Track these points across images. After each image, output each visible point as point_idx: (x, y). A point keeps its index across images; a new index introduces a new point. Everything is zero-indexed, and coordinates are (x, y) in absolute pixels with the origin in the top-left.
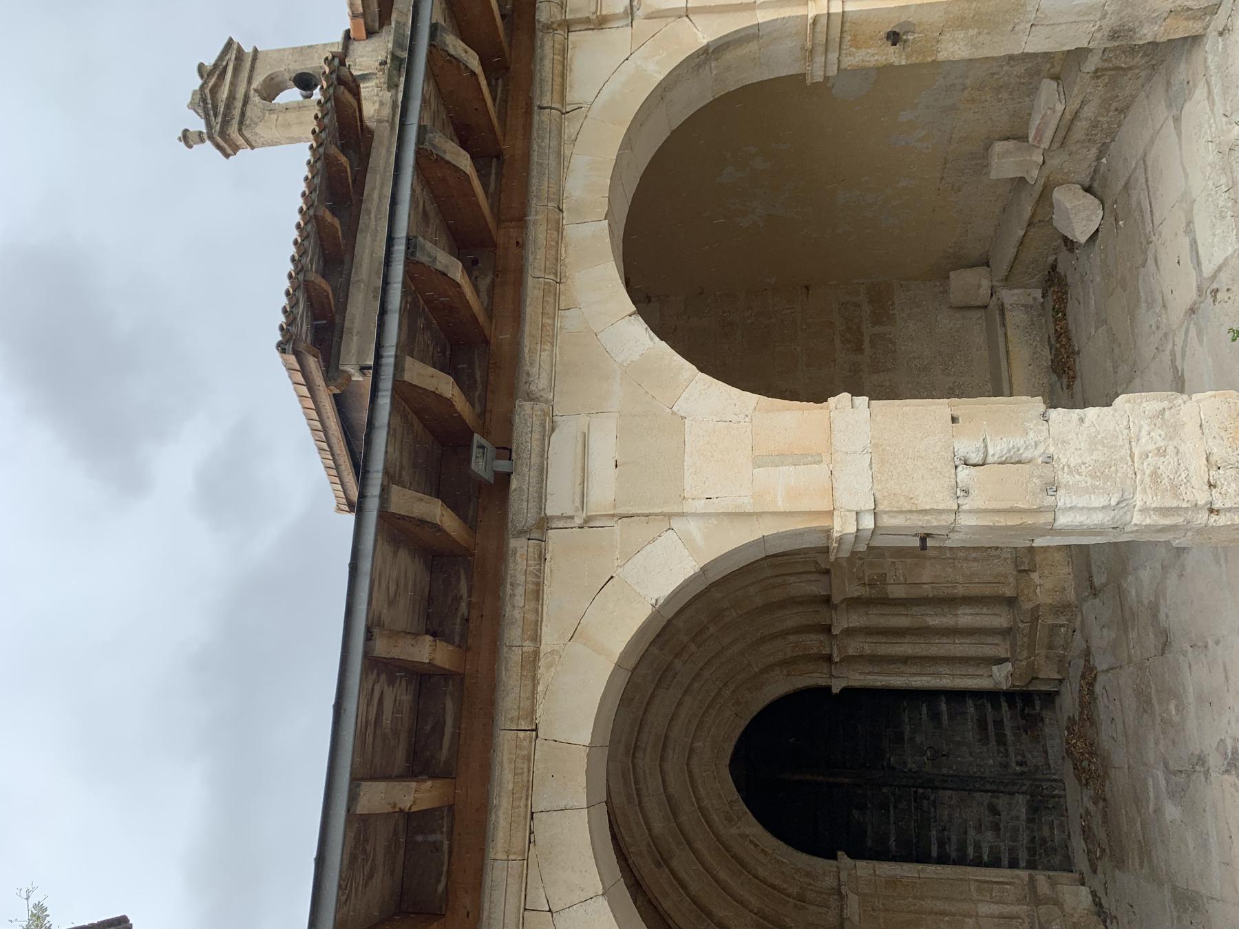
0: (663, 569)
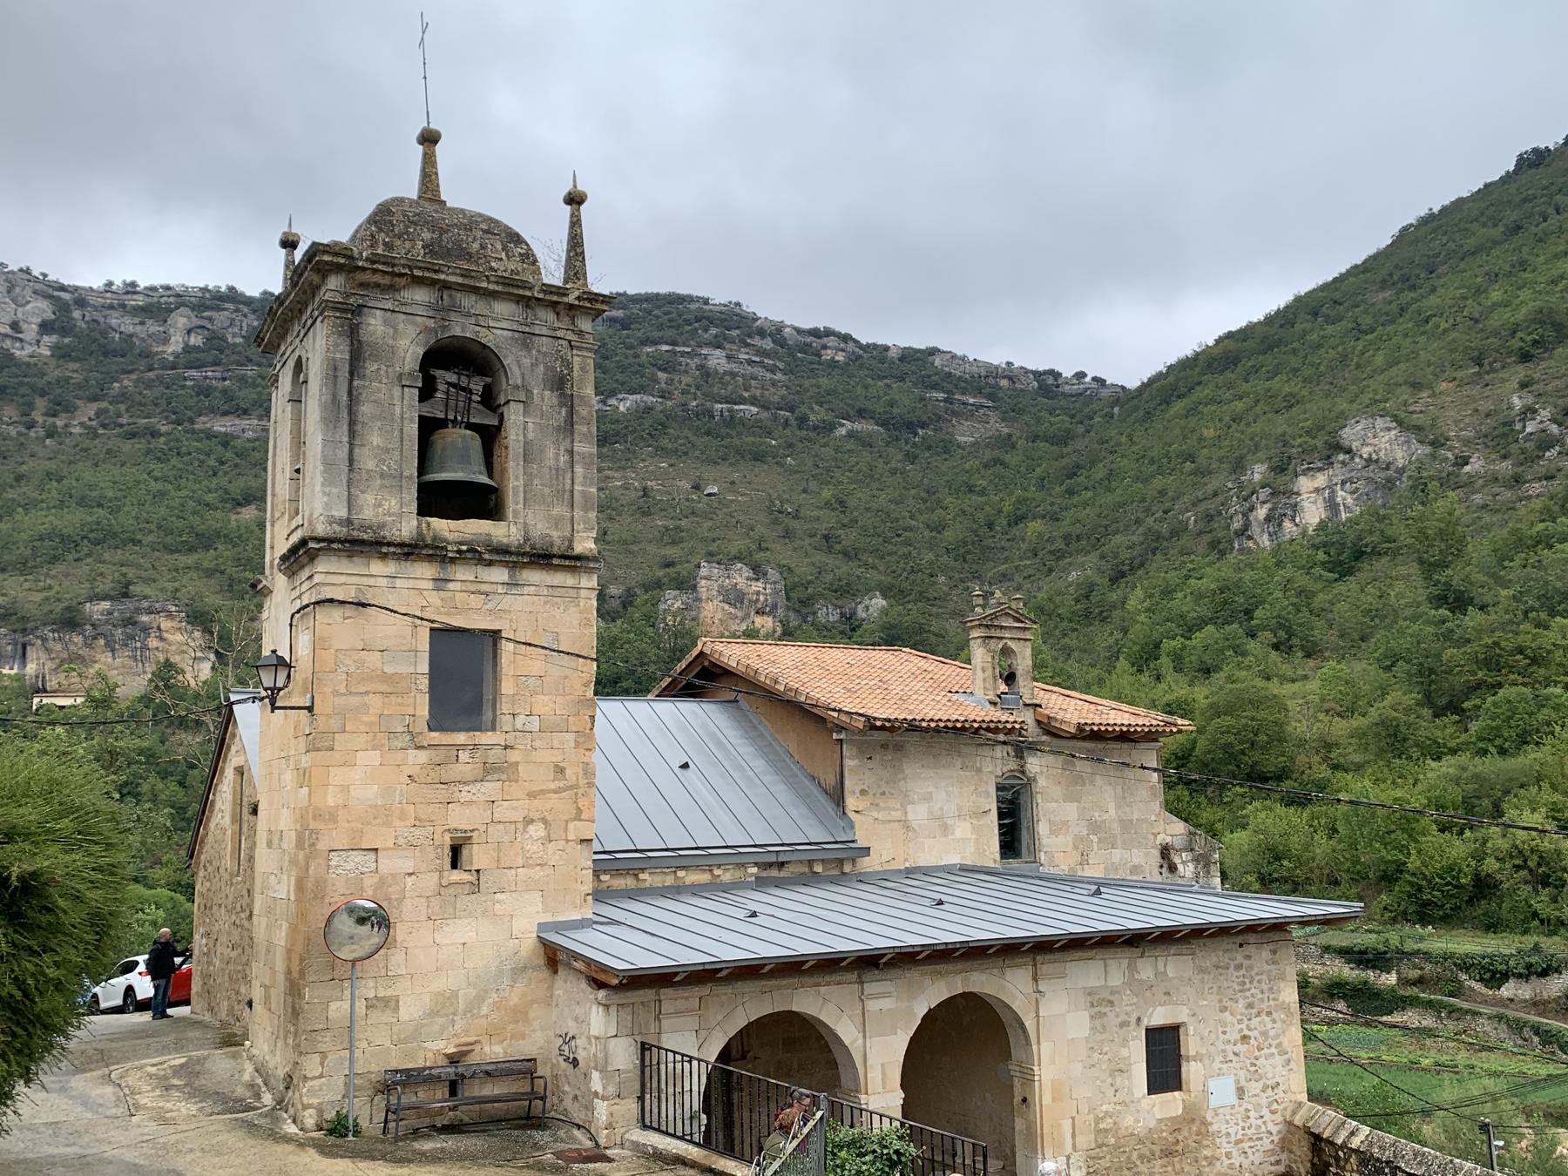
0: (846, 1031)
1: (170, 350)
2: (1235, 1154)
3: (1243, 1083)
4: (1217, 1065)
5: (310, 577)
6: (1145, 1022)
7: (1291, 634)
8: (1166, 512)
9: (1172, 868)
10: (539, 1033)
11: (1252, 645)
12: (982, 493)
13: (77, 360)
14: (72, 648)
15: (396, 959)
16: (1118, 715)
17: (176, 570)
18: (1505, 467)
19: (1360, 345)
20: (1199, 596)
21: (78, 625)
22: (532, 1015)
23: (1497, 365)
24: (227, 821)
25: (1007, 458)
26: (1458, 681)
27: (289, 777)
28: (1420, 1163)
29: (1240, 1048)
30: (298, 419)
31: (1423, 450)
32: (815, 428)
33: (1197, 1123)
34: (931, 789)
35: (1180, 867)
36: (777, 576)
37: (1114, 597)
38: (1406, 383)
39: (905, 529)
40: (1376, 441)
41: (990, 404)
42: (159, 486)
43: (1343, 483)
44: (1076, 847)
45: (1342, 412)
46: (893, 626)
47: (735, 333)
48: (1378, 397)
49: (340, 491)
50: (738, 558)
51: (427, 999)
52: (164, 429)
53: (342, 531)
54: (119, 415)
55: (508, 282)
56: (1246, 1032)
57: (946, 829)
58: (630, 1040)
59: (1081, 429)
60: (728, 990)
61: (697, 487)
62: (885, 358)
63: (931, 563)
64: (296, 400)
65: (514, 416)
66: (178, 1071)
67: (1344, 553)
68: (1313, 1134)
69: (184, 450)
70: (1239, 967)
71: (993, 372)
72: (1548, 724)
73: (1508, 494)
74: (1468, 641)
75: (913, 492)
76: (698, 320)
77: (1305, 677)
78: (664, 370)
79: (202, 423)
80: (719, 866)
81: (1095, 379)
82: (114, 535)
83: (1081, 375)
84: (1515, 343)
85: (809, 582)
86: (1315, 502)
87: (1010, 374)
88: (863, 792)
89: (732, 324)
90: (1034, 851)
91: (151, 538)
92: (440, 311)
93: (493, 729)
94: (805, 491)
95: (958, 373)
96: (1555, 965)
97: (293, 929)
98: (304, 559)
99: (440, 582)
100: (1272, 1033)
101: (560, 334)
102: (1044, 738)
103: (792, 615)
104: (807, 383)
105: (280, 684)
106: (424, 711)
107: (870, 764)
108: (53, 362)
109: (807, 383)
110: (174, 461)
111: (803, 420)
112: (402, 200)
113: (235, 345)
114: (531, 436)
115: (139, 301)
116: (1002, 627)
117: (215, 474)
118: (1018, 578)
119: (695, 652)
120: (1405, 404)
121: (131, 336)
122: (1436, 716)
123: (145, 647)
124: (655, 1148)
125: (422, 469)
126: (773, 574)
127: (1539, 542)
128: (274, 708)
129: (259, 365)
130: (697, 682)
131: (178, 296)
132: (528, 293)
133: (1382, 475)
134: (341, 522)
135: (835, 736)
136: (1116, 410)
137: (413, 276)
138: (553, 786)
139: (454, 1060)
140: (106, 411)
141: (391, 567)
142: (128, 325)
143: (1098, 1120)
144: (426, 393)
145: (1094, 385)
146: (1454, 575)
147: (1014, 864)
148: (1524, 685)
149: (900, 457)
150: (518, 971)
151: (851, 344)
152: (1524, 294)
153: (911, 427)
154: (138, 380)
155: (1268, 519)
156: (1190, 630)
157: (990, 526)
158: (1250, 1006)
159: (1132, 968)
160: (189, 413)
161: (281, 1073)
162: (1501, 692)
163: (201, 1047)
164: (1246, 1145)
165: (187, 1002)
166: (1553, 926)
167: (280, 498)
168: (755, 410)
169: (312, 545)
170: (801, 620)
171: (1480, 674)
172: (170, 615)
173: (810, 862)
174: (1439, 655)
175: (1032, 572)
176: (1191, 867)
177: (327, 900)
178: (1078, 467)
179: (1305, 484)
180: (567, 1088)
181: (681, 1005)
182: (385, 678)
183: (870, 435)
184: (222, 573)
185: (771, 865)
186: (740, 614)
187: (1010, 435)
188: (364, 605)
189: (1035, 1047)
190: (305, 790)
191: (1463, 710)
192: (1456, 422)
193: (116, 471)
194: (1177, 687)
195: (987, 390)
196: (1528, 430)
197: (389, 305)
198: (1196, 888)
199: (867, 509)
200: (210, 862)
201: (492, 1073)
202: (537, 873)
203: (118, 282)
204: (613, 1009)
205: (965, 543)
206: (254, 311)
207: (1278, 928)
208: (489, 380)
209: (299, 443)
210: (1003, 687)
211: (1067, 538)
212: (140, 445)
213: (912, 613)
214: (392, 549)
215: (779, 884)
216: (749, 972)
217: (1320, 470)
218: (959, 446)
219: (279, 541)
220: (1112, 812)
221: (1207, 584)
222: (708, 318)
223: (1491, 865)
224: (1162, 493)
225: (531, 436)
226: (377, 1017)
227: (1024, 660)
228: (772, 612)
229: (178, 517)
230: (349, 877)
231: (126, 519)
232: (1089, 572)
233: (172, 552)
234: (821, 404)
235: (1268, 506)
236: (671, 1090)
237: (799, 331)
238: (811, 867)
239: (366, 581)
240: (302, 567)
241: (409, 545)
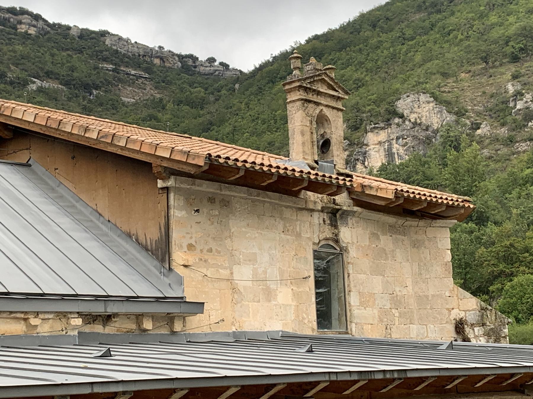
18: (503, 132)
19: (405, 48)
23: (497, 63)
25: (160, 115)
26: (486, 271)
31: (450, 118)
32: (11, 83)
34: (256, 250)
38: (438, 72)
40: (419, 110)
41: (147, 76)
43: (398, 138)
44: (381, 321)
45: (397, 90)
48: (421, 80)
57: (270, 295)
59: (212, 98)
62: (69, 34)
73: (504, 151)
80: (37, 314)
81: (221, 64)
83: (212, 60)
84: (508, 50)
86: (378, 151)
87: (161, 55)
95: (123, 51)
102: (356, 208)
107: (198, 217)
116: (319, 93)
120: (439, 86)
127: (527, 182)
133: (423, 134)
135: (160, 184)
136: (237, 86)
145: (221, 68)
147: (329, 334)
151: (41, 22)
152: (511, 19)
153: (87, 87)
162: (516, 279)
174: (472, 254)
178: (211, 124)
179: (372, 138)
183: (56, 91)
187: (161, 100)
192: (472, 100)
195: (145, 65)
196: (518, 107)
217: (382, 129)
218: (123, 104)
220: (410, 288)
234: (17, 65)
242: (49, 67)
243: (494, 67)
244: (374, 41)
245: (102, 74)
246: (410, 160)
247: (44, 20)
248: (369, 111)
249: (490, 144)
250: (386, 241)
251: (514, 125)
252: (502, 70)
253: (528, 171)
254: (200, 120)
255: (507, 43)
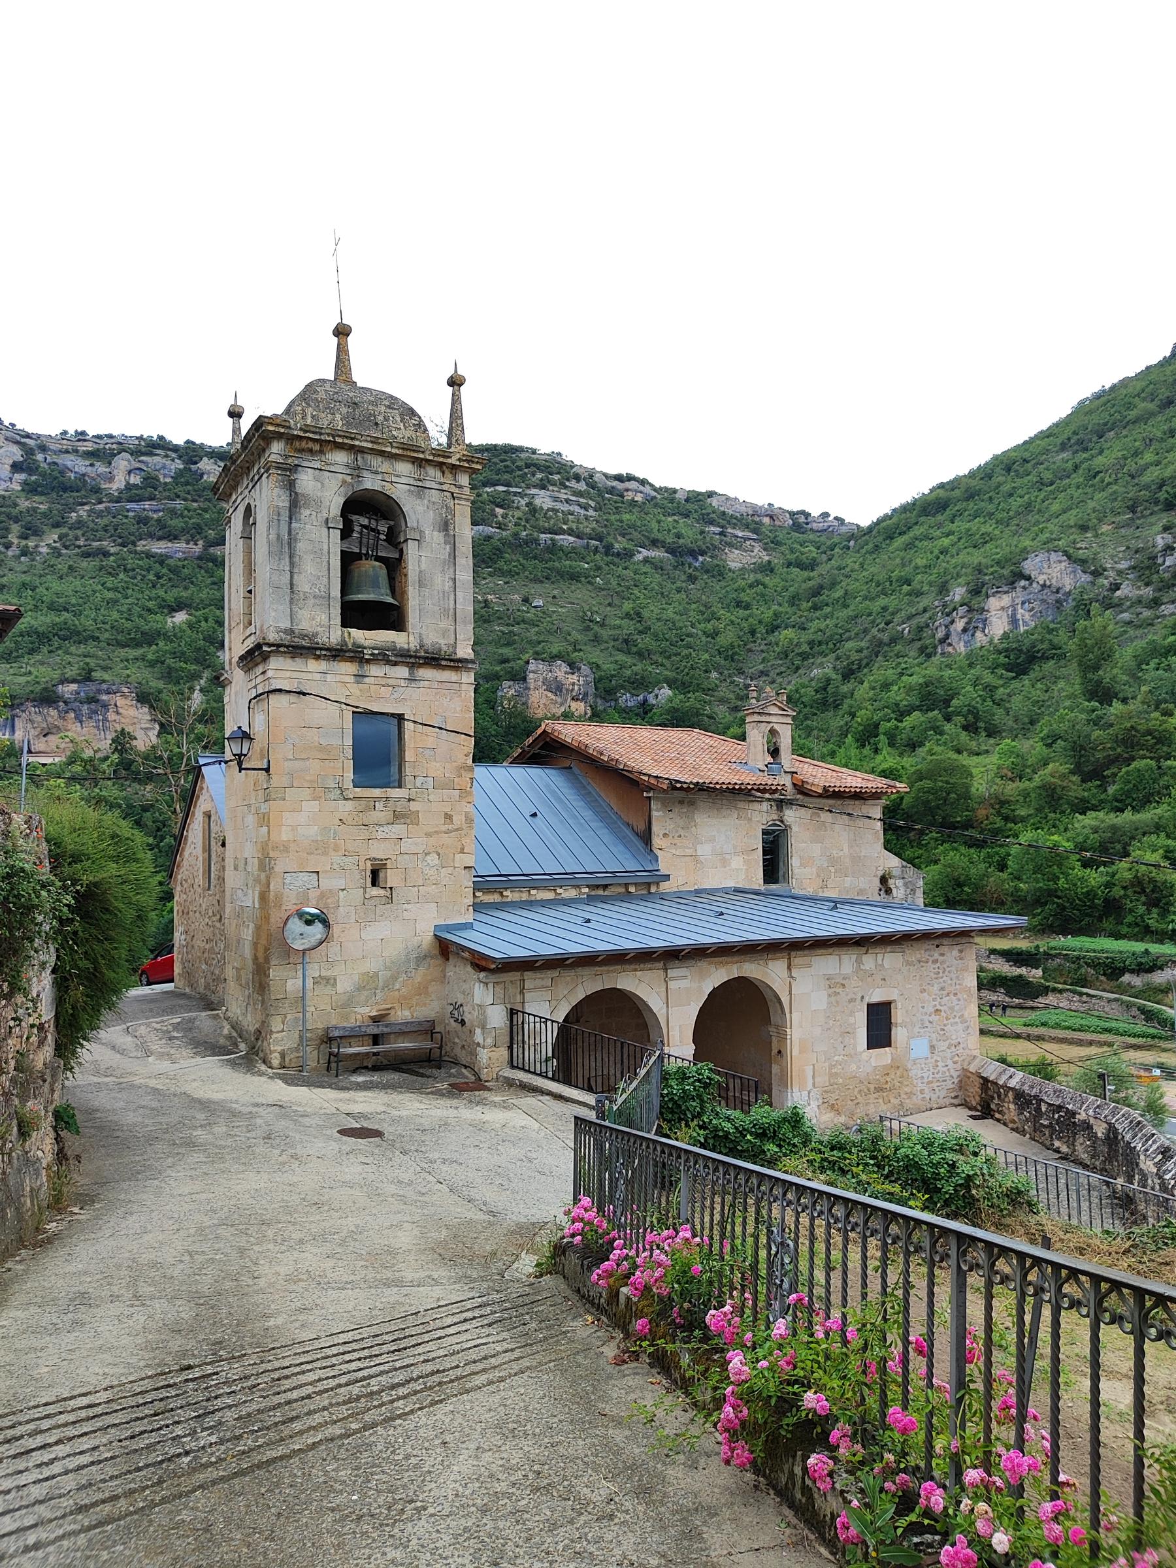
0: (655, 1003)
1: (115, 488)
2: (927, 1091)
3: (935, 1042)
4: (916, 1029)
5: (264, 673)
6: (867, 1000)
7: (977, 717)
8: (887, 624)
9: (888, 891)
10: (436, 1003)
11: (948, 727)
12: (747, 607)
13: (42, 494)
14: (49, 719)
15: (333, 949)
16: (854, 780)
17: (127, 660)
18: (1148, 592)
19: (1042, 495)
20: (910, 689)
21: (55, 702)
22: (430, 989)
24: (199, 851)
25: (767, 580)
27: (251, 820)
28: (1058, 1097)
29: (934, 1018)
30: (249, 553)
32: (618, 554)
33: (901, 1069)
35: (894, 891)
36: (589, 671)
37: (845, 689)
39: (688, 636)
40: (1049, 571)
41: (755, 537)
42: (110, 595)
43: (1023, 603)
44: (818, 876)
45: (1025, 548)
46: (676, 710)
47: (557, 477)
49: (285, 607)
50: (558, 657)
51: (356, 978)
52: (112, 550)
53: (286, 639)
54: (77, 539)
55: (405, 447)
56: (938, 1007)
57: (725, 863)
58: (503, 1007)
60: (572, 973)
61: (526, 600)
63: (706, 661)
64: (247, 537)
65: (411, 549)
66: (176, 1027)
67: (1020, 659)
68: (982, 1078)
69: (129, 566)
70: (936, 961)
71: (756, 511)
72: (1167, 787)
73: (1147, 613)
74: (1112, 725)
75: (694, 606)
76: (528, 466)
77: (987, 752)
78: (501, 507)
79: (142, 546)
80: (561, 887)
81: (836, 518)
82: (78, 633)
83: (825, 515)
85: (613, 676)
87: (772, 513)
88: (665, 835)
89: (553, 470)
90: (787, 880)
91: (107, 635)
92: (356, 471)
93: (400, 787)
94: (610, 605)
95: (731, 512)
96: (1159, 963)
97: (258, 928)
98: (259, 659)
99: (359, 677)
100: (957, 1008)
101: (445, 487)
103: (599, 701)
104: (613, 518)
105: (244, 752)
106: (349, 775)
107: (671, 815)
108: (23, 494)
109: (613, 518)
110: (121, 576)
111: (608, 549)
112: (324, 381)
113: (166, 483)
114: (423, 566)
115: (89, 446)
116: (770, 714)
117: (154, 586)
118: (773, 674)
119: (539, 731)
121: (84, 475)
122: (1083, 781)
123: (105, 720)
124: (521, 1081)
125: (344, 591)
126: (585, 669)
128: (241, 770)
129: (185, 500)
130: (542, 752)
131: (120, 443)
132: (421, 456)
134: (285, 632)
136: (852, 543)
137: (335, 442)
138: (444, 828)
139: (376, 1020)
140: (67, 535)
141: (323, 665)
142: (79, 466)
143: (831, 1067)
144: (346, 534)
145: (836, 523)
146: (1106, 674)
148: (1151, 758)
149: (683, 577)
150: (421, 958)
153: (694, 554)
154: (91, 511)
155: (965, 630)
156: (902, 714)
157: (753, 633)
158: (942, 989)
159: (859, 962)
160: (133, 538)
161: (252, 1029)
163: (190, 1011)
164: (935, 1085)
165: (172, 981)
166: (1162, 937)
167: (234, 612)
168: (572, 539)
169: (265, 648)
170: (609, 700)
171: (1119, 750)
172: (123, 695)
173: (626, 885)
175: (783, 669)
176: (902, 890)
177: (284, 908)
179: (994, 603)
180: (457, 1040)
181: (539, 983)
182: (321, 748)
184: (163, 663)
185: (598, 887)
186: (559, 700)
187: (769, 562)
188: (304, 694)
189: (788, 1016)
190: (265, 829)
191: (1104, 777)
192: (1112, 557)
193: (78, 583)
194: (888, 758)
196: (1167, 563)
197: (317, 465)
198: (906, 905)
199: (659, 620)
200: (186, 881)
201: (405, 1031)
202: (433, 889)
203: (71, 432)
204: (491, 986)
205: (733, 647)
206: (180, 457)
207: (962, 935)
208: (392, 523)
209: (250, 570)
210: (769, 759)
211: (811, 643)
212: (95, 563)
213: (692, 700)
214: (324, 652)
215: (603, 900)
216: (588, 960)
217: (1006, 592)
218: (730, 570)
219: (236, 644)
221: (915, 680)
222: (535, 465)
223: (1117, 892)
224: (885, 609)
225: (423, 566)
226: (319, 990)
227: (785, 740)
228: (584, 698)
229: (127, 619)
230: (293, 889)
231: (86, 622)
232: (826, 670)
233: (124, 646)
235: (965, 620)
236: (532, 1042)
237: (606, 475)
238: (627, 889)
239: (304, 675)
240: (257, 665)
241: (337, 650)
242: (656, 535)
243: (1143, 517)
244: (1006, 488)
245: (708, 539)
246: (1036, 627)
247: (651, 485)
248: (992, 573)
249: (1131, 606)
250: (825, 817)
251: (1161, 584)
252: (1153, 519)
253: (1172, 638)
254: (811, 584)
255: (1161, 487)
